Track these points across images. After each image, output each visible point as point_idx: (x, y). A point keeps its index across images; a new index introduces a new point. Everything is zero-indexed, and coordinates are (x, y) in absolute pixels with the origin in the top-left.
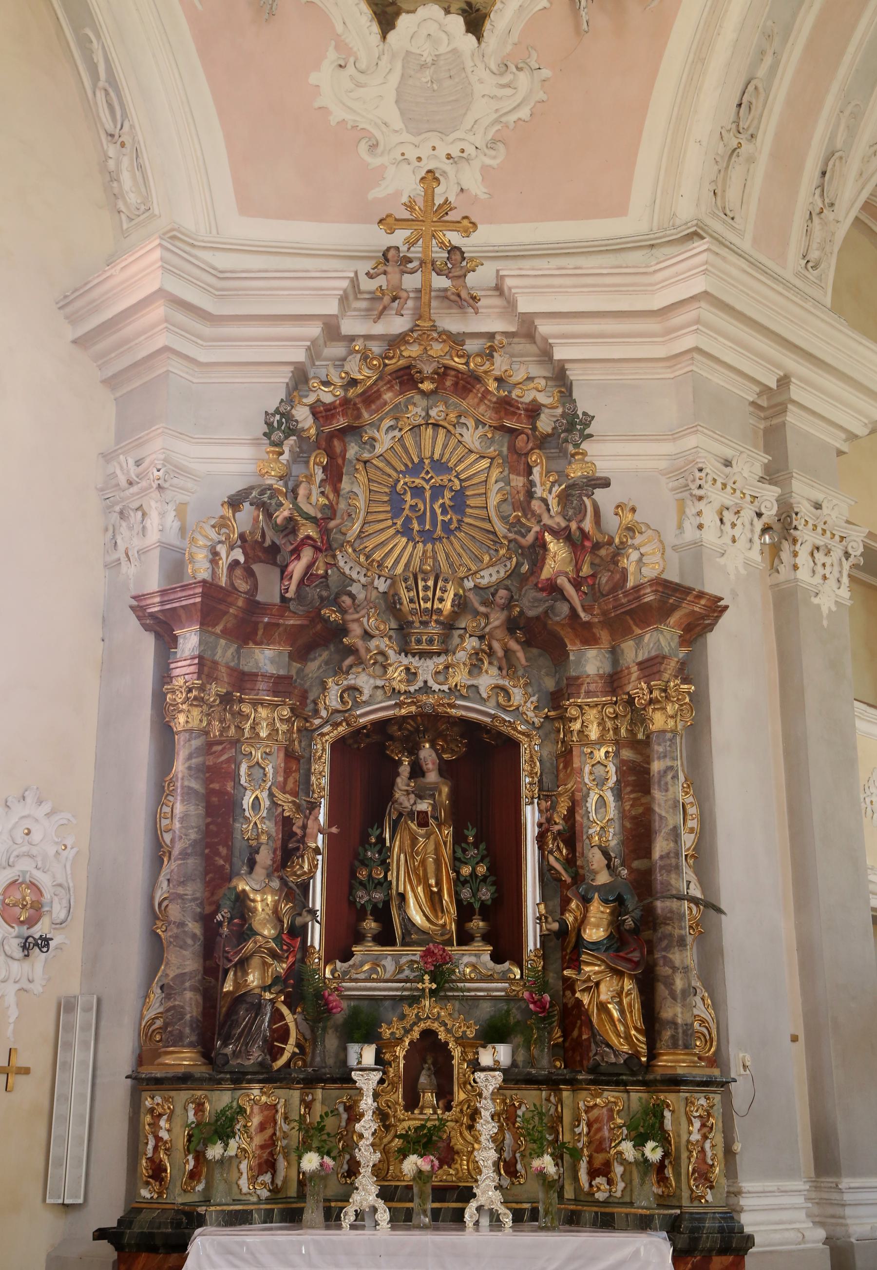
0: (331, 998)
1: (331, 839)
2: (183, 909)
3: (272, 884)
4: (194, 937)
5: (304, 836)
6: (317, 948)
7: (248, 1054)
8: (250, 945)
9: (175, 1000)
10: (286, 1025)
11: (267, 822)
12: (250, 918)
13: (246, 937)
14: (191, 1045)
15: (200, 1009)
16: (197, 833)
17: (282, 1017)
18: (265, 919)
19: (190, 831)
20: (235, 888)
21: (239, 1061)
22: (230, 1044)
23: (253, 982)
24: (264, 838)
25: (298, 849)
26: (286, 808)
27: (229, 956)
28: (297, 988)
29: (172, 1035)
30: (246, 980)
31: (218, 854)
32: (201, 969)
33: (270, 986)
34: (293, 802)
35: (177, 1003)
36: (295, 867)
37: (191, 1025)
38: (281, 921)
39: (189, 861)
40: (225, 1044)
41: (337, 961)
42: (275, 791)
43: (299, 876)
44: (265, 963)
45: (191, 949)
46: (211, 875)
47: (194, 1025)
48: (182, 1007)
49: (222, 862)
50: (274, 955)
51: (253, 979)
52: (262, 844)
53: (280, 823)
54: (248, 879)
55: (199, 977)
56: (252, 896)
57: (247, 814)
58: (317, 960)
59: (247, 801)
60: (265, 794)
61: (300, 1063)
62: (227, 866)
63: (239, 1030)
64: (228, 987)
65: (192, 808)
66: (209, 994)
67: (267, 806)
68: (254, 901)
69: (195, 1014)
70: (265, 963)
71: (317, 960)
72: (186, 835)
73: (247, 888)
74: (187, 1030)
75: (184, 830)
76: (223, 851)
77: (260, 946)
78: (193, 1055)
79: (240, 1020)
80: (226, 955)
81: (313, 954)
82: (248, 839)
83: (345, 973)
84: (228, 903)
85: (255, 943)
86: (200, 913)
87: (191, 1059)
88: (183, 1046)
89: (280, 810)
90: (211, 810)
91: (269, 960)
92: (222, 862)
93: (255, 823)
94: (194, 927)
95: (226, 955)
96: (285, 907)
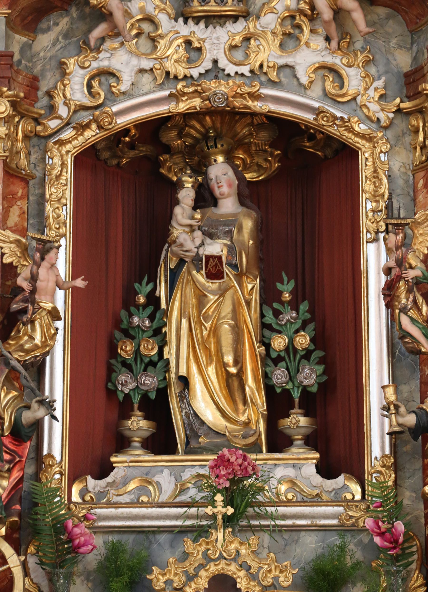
0: (77, 531)
5: (34, 291)
6: (58, 458)
25: (24, 311)
34: (17, 242)
36: (20, 338)
41: (89, 478)
43: (28, 352)
58: (57, 476)
81: (51, 466)
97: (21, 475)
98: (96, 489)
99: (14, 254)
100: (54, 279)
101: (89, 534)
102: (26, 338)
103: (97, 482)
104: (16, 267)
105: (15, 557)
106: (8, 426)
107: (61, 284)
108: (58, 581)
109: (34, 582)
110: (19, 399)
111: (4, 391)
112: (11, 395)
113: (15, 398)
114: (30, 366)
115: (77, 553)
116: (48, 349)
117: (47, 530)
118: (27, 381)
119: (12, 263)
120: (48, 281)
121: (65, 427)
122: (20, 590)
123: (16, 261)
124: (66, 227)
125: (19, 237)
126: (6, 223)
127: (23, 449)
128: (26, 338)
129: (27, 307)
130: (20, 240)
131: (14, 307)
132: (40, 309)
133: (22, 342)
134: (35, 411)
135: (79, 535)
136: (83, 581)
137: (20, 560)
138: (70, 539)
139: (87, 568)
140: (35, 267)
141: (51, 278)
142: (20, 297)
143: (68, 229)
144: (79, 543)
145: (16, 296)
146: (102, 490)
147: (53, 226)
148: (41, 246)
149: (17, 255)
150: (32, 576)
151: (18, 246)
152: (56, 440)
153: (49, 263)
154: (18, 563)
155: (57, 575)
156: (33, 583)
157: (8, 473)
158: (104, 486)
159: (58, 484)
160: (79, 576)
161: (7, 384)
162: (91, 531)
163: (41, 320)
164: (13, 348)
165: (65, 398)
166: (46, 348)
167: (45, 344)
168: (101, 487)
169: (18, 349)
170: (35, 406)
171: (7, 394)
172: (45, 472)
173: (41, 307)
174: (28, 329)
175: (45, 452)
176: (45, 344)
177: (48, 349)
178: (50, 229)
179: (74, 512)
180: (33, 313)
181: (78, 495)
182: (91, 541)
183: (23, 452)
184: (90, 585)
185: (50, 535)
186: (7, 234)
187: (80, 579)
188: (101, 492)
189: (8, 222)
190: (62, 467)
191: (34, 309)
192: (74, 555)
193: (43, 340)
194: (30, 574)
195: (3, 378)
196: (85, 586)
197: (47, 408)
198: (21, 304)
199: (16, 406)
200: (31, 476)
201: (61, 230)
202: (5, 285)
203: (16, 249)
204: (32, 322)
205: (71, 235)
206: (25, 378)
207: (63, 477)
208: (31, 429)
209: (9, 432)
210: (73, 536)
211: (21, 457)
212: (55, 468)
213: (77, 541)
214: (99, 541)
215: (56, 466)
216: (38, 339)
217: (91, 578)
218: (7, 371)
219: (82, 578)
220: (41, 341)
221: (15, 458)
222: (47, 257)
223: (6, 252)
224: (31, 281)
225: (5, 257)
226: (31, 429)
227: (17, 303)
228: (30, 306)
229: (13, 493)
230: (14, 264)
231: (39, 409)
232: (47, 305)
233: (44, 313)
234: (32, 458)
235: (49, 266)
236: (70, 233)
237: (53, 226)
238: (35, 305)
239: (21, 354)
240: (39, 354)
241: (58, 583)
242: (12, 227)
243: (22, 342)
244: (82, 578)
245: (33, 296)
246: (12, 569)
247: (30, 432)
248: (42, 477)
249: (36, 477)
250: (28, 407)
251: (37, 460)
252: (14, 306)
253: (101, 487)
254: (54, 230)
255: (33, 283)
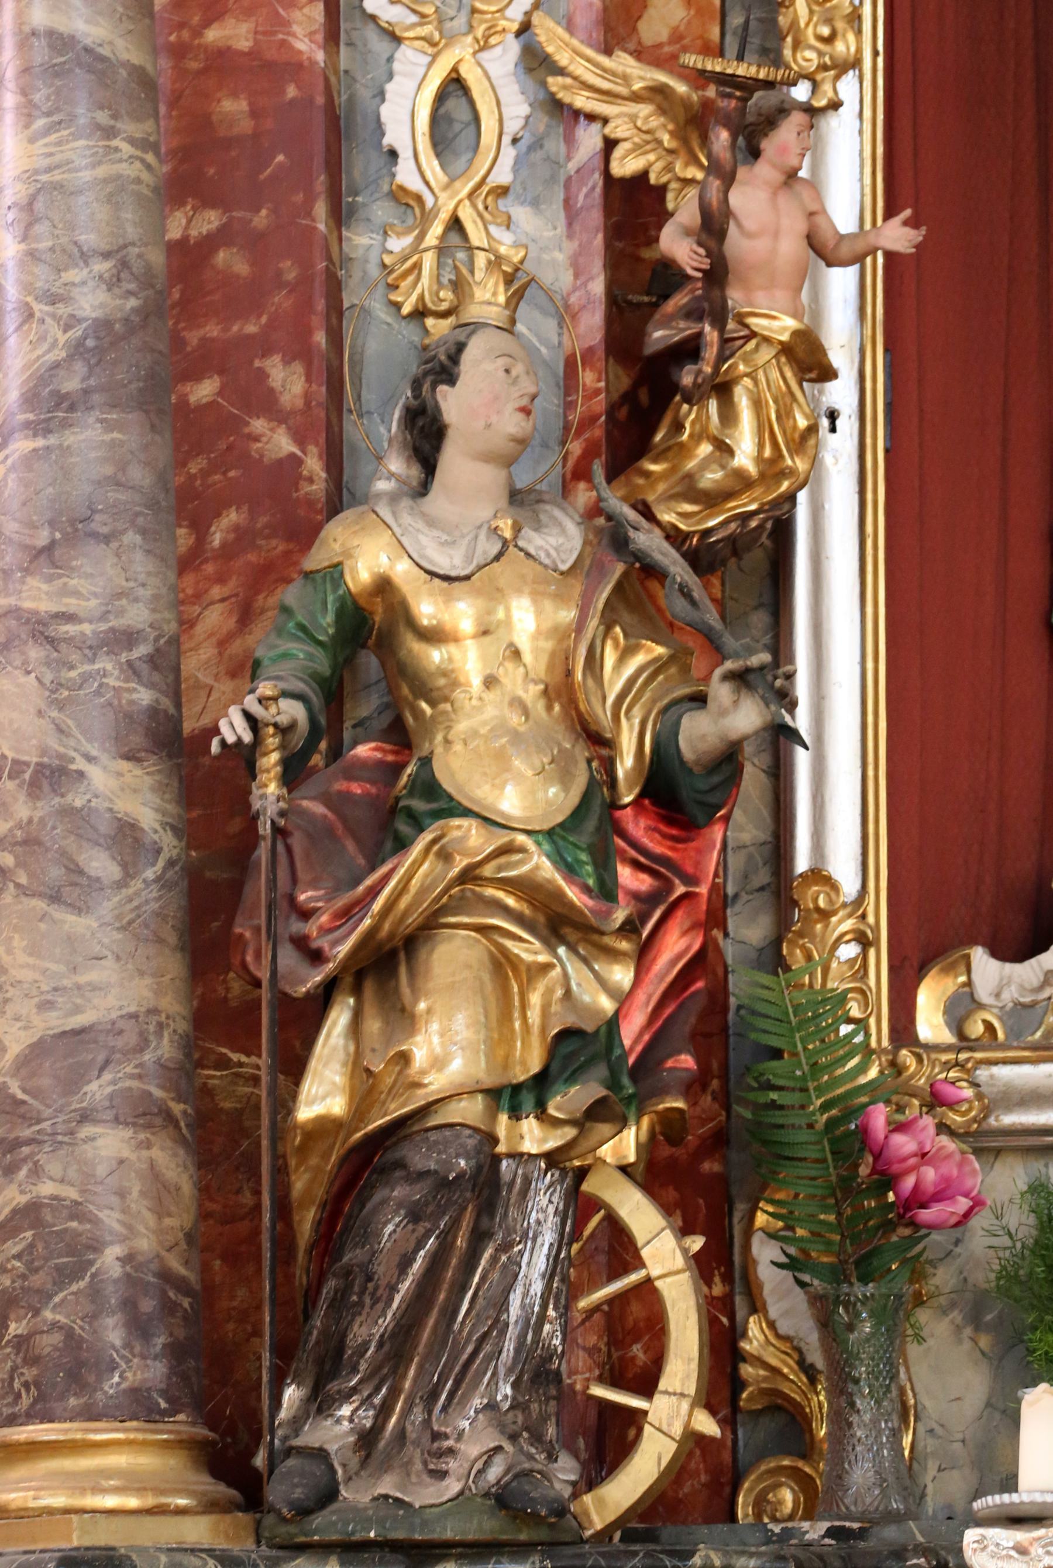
0: (904, 1144)
1: (905, 295)
2: (58, 696)
3: (534, 541)
4: (126, 837)
5: (717, 274)
6: (849, 885)
7: (438, 1452)
8: (414, 873)
9: (37, 1172)
10: (647, 1288)
11: (521, 214)
12: (427, 726)
13: (403, 827)
14: (138, 1406)
15: (181, 1218)
16: (112, 283)
17: (619, 1249)
18: (500, 727)
19: (74, 275)
20: (335, 572)
21: (387, 1486)
22: (346, 1396)
23: (438, 1063)
24: (488, 297)
25: (688, 350)
26: (618, 129)
27: (311, 928)
28: (723, 1104)
29: (32, 1361)
30: (404, 1058)
31: (266, 403)
32: (175, 1006)
33: (542, 1083)
34: (658, 94)
35: (47, 1189)
36: (684, 451)
37: (129, 1305)
38: (599, 742)
39: (71, 438)
40: (320, 1403)
41: (979, 955)
42: (550, 35)
43: (712, 500)
44: (503, 965)
45: (108, 906)
46: (232, 517)
47: (148, 1305)
48: (76, 1210)
49: (281, 443)
50: (557, 923)
51: (448, 1047)
52: (474, 327)
53: (595, 217)
54: (407, 519)
55: (165, 1049)
56: (426, 609)
57: (406, 175)
58: (849, 951)
59: (404, 111)
60: (504, 58)
61: (787, 1496)
62: (314, 464)
63: (386, 1321)
64: (323, 1095)
65: (79, 150)
66: (223, 1132)
67: (513, 126)
68: (434, 636)
69: (145, 1244)
70: (503, 965)
71: (849, 951)
72: (54, 299)
73: (401, 570)
74: (113, 1332)
75: (42, 275)
76: (288, 381)
77: (469, 875)
78: (146, 1461)
79: (383, 1269)
80: (297, 927)
81: (825, 915)
82: (420, 313)
83: (1022, 1013)
84: (300, 650)
85: (445, 856)
86: (153, 712)
87: (131, 1483)
88: (90, 1414)
89: (589, 139)
90: (193, 165)
91: (529, 950)
92: (281, 443)
93: (455, 224)
94: (126, 791)
95: (297, 927)
96: (624, 666)
97: (696, 946)
98: (1010, 995)
99: (650, 141)
100: (801, 226)
101: (958, 1157)
102: (705, 449)
103: (1009, 967)
104: (663, 189)
105: (668, 1241)
106: (634, 768)
107: (831, 243)
108: (850, 1328)
109: (781, 1332)
110: (673, 670)
111: (616, 644)
112: (639, 659)
113: (658, 667)
114: (727, 552)
115: (914, 1224)
116: (785, 485)
117: (807, 1143)
118: (693, 603)
119: (644, 175)
120: (776, 235)
121: (871, 773)
122: (690, 1360)
123: (659, 166)
124: (859, 32)
125: (662, 77)
126: (634, 29)
127: (699, 851)
128: (705, 449)
129: (699, 335)
130: (667, 86)
131: (660, 336)
132: (748, 338)
133: (691, 465)
134: (723, 713)
135: (913, 1161)
136: (958, 1329)
137: (685, 1251)
138: (882, 1173)
139: (970, 1281)
140: (715, 184)
141: (786, 222)
142: (680, 300)
143: (868, 42)
144: (916, 1187)
145: (666, 297)
146: (1027, 999)
147: (810, 31)
148: (733, 103)
149: (660, 142)
150: (773, 1312)
151: (662, 111)
152: (839, 821)
153: (774, 166)
154: (680, 1262)
155: (847, 1305)
156: (778, 1336)
157: (629, 940)
158: (1036, 983)
159: (853, 977)
160: (944, 1312)
161: (626, 617)
162: (964, 1147)
163: (756, 382)
164: (661, 487)
165: (870, 665)
166: (779, 484)
167: (772, 469)
168: (1022, 987)
169: (677, 489)
170: (721, 692)
171: (625, 654)
172: (801, 934)
173: (753, 335)
174: (708, 417)
175: (802, 863)
176: (777, 469)
177: (785, 485)
178: (797, 45)
179: (912, 1077)
180: (722, 358)
181: (939, 1019)
182: (969, 1183)
183: (697, 864)
184: (985, 1341)
185: (817, 1161)
186: (620, 69)
187: (947, 1320)
188: (1025, 1006)
189: (642, 26)
190: (864, 916)
191: (725, 341)
192: (907, 1232)
193: (767, 453)
194: (764, 1304)
195: (605, 595)
196: (967, 1345)
197: (763, 698)
198: (682, 324)
199: (660, 698)
200: (761, 950)
201: (840, 47)
202: (639, 259)
203: (655, 122)
204: (723, 389)
205: (880, 60)
206: (685, 592)
207: (872, 952)
208: (716, 779)
209: (637, 791)
210: (889, 1163)
211: (691, 880)
212: (840, 922)
213: (909, 1183)
214: (1006, 1182)
215: (841, 914)
216: (745, 453)
217: (989, 1317)
218: (619, 569)
219: (956, 1315)
220: (759, 459)
221: (669, 887)
222: (769, 146)
223: (619, 134)
224: (704, 236)
225: (618, 152)
226: (716, 779)
227: (666, 323)
228: (707, 328)
229: (668, 1011)
230: (653, 179)
231: (736, 702)
232: (776, 324)
233: (766, 354)
234: (762, 889)
235: (778, 177)
236: (876, 54)
237: (810, 31)
238: (731, 325)
239: (688, 508)
240: (753, 507)
241: (852, 1337)
242: (660, 45)
243: (691, 465)
244: (956, 1315)
245: (716, 293)
246: (658, 1284)
247: (713, 789)
248: (791, 953)
249: (773, 959)
250: (699, 700)
251: (777, 894)
252: (658, 334)
253: (1022, 987)
254: (811, 47)
255: (712, 244)
